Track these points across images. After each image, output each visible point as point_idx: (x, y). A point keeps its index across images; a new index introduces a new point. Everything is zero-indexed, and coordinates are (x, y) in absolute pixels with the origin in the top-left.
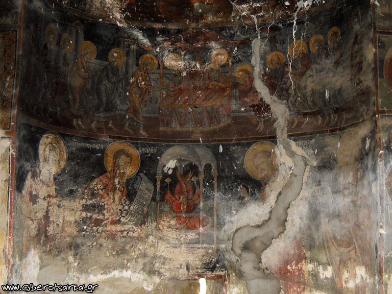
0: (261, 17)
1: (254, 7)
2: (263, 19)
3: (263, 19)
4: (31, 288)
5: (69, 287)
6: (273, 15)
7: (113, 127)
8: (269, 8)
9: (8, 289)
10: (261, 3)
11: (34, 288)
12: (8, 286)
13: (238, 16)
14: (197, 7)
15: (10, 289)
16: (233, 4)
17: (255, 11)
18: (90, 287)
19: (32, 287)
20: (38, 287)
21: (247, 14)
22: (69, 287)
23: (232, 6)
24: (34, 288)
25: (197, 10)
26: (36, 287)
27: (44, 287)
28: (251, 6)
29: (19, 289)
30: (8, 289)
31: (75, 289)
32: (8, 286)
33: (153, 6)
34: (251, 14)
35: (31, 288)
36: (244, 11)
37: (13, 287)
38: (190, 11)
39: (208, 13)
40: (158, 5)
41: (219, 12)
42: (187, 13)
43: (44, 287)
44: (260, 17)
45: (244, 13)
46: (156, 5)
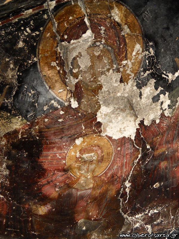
0: (158, 224)
1: (150, 215)
2: (160, 227)
3: (160, 227)
4: (137, 236)
5: (161, 235)
6: (173, 219)
7: (128, 194)
8: (169, 212)
9: (123, 236)
10: (159, 208)
11: (139, 236)
12: (123, 235)
13: (129, 229)
14: (81, 224)
15: (124, 236)
16: (125, 216)
17: (150, 220)
18: (173, 235)
19: (138, 235)
20: (142, 235)
21: (141, 226)
22: (161, 235)
23: (123, 219)
24: (139, 236)
25: (80, 227)
26: (141, 235)
27: (145, 235)
28: (147, 214)
29: (130, 236)
30: (123, 236)
31: (164, 236)
32: (123, 235)
33: (28, 221)
34: (146, 224)
35: (137, 236)
36: (137, 222)
37: (127, 235)
38: (71, 228)
39: (93, 230)
40: (34, 221)
41: (107, 228)
42: (68, 231)
43: (145, 235)
44: (156, 225)
45: (138, 225)
46: (31, 220)
